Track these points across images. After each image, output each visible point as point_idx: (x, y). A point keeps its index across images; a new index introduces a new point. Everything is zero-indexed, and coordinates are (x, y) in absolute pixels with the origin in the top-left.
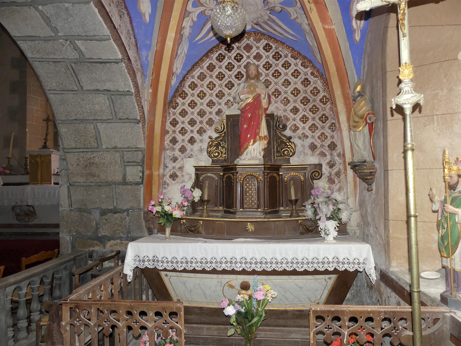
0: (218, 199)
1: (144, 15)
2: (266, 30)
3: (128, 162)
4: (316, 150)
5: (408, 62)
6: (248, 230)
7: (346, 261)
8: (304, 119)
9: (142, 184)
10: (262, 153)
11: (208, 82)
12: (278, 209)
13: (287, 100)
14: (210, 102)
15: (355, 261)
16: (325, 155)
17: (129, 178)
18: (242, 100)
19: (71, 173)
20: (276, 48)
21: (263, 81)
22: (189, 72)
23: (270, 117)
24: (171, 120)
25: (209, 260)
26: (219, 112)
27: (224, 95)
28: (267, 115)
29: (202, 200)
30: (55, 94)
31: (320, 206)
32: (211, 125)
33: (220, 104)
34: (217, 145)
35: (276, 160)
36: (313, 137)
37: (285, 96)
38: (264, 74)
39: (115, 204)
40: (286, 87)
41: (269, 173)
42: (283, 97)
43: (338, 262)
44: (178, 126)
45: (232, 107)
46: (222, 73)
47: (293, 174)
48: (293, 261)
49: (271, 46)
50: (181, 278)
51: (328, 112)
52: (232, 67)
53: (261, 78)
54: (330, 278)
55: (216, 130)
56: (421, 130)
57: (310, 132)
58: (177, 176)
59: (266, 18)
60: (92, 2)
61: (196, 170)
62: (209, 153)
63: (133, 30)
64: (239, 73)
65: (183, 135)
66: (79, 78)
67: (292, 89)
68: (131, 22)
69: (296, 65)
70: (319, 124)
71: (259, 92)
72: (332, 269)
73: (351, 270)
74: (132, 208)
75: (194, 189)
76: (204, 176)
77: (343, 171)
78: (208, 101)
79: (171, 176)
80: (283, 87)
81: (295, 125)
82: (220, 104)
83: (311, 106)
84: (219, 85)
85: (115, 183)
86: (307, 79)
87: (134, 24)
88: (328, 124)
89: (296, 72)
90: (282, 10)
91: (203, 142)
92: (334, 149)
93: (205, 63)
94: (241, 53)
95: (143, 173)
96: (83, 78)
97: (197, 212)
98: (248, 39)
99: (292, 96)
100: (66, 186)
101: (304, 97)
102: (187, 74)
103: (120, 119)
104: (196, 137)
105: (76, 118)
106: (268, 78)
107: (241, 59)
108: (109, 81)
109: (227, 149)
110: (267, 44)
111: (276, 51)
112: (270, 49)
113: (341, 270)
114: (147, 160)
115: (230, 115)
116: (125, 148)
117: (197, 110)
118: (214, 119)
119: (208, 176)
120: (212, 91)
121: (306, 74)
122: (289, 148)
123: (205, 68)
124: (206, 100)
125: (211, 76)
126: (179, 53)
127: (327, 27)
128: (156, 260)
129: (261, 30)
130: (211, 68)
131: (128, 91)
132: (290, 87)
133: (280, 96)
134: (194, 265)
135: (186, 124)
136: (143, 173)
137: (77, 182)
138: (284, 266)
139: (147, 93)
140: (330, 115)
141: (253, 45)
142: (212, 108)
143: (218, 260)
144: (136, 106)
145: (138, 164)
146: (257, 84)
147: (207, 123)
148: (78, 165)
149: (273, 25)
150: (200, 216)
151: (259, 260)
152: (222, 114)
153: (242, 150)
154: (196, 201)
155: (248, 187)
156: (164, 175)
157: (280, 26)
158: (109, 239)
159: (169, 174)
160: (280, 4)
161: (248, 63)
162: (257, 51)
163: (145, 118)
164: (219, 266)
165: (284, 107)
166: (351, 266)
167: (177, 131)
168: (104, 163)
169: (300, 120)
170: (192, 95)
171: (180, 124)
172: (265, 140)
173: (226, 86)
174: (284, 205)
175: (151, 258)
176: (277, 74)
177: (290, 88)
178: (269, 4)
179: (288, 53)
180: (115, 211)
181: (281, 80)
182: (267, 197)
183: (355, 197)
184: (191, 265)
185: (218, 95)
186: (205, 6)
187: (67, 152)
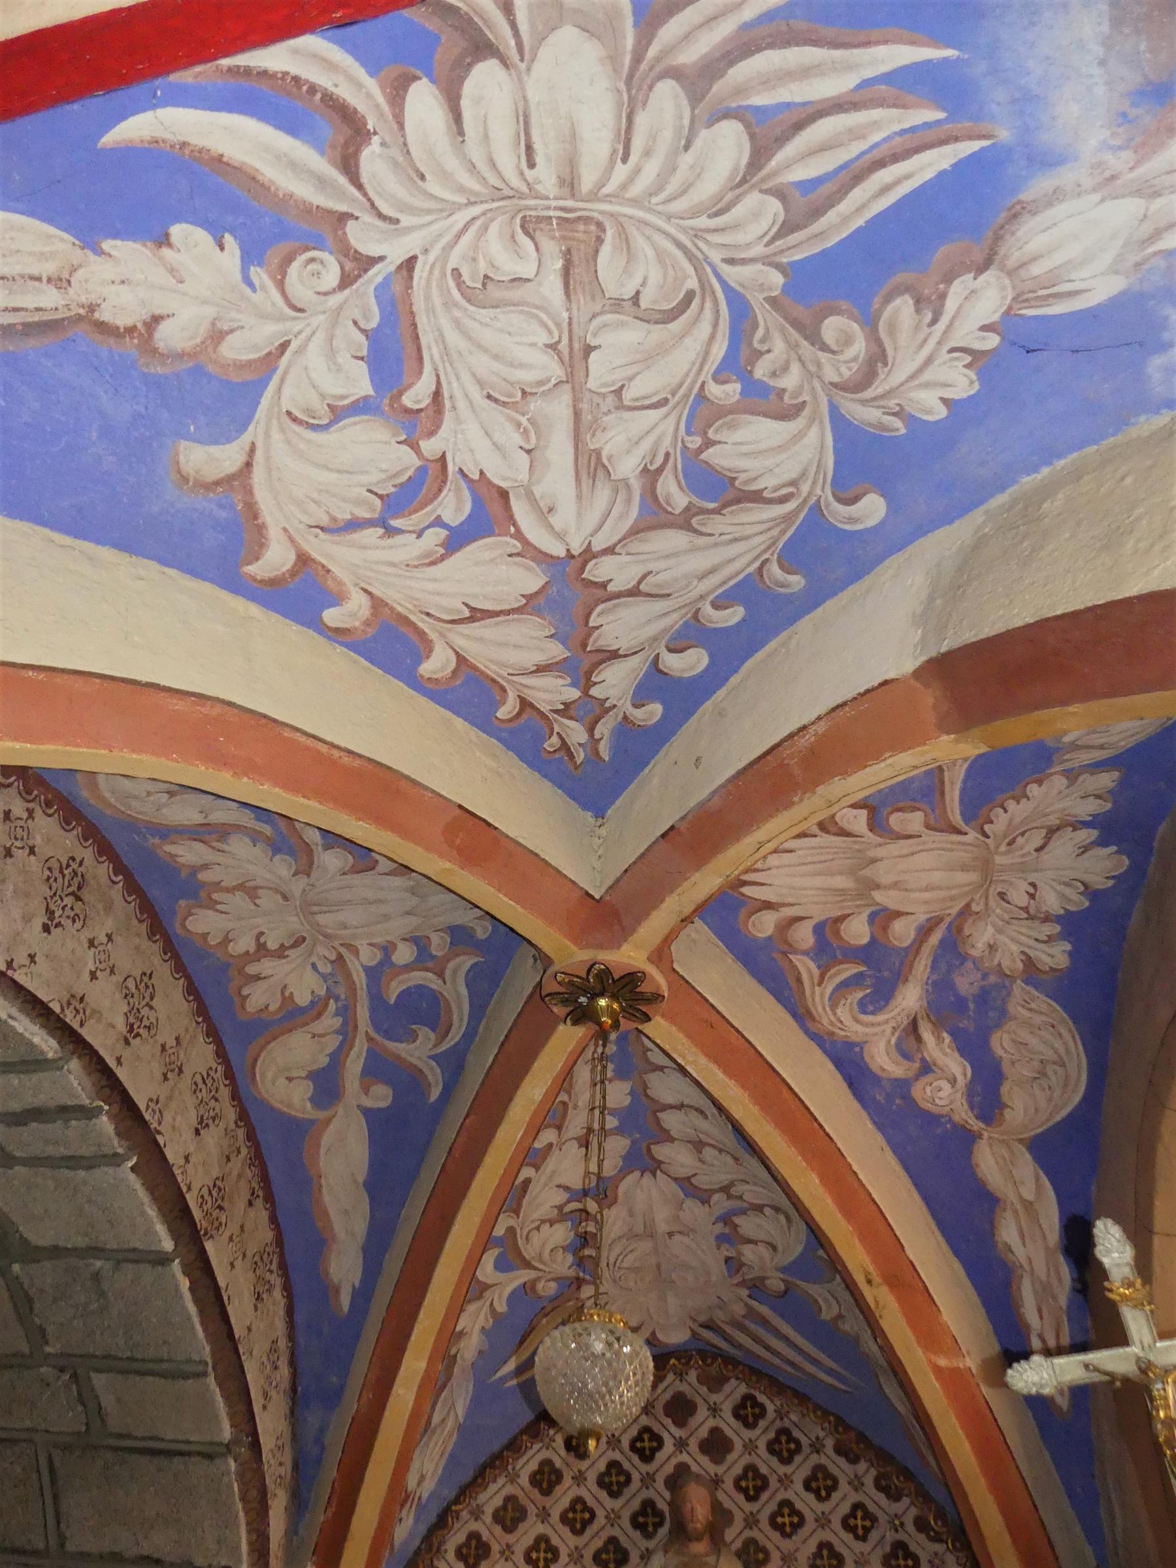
1: (337, 1291)
2: (740, 1346)
20: (780, 1415)
21: (738, 1544)
22: (466, 1491)
52: (615, 1488)
59: (739, 1310)
60: (177, 1261)
63: (291, 1337)
69: (857, 1484)
87: (299, 1318)
90: (786, 1292)
93: (525, 1458)
94: (657, 1428)
98: (681, 1375)
102: (457, 1501)
106: (754, 1533)
107: (654, 1451)
111: (778, 1424)
123: (524, 1480)
125: (544, 1515)
126: (436, 1419)
127: (943, 1362)
141: (699, 1401)
149: (761, 1332)
160: (784, 1270)
162: (711, 1423)
178: (745, 1269)
179: (822, 1434)
186: (536, 1269)
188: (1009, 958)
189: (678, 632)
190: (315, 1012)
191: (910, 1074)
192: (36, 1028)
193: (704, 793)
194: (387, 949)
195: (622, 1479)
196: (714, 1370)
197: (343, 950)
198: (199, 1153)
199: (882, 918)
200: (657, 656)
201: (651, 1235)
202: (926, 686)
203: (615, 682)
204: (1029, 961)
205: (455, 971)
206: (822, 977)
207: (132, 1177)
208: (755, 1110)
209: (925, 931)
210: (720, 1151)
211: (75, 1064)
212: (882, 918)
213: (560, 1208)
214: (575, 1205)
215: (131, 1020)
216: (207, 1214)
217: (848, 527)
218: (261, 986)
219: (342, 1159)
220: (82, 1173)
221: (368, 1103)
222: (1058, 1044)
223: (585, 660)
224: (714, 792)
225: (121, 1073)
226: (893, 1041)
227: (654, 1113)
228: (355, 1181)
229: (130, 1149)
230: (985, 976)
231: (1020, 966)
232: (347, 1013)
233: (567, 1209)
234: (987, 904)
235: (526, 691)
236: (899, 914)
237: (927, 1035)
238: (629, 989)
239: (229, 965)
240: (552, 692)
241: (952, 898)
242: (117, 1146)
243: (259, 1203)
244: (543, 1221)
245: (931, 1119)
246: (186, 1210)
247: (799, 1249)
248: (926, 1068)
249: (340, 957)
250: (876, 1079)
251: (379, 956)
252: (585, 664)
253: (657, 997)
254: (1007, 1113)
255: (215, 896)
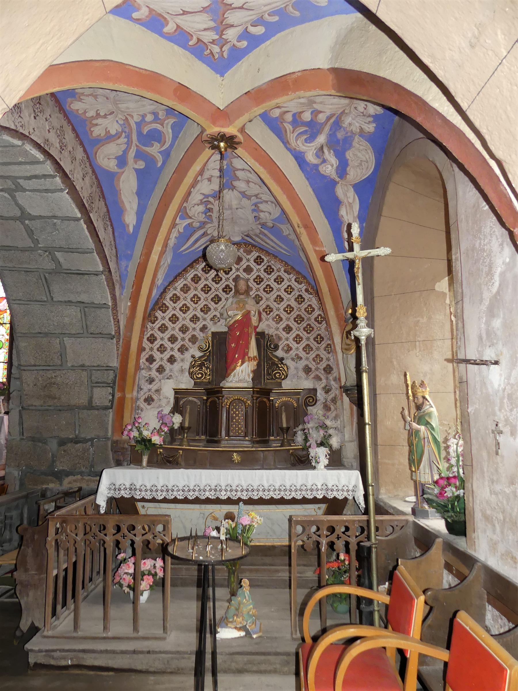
0: (201, 426)
1: (128, 226)
2: (258, 242)
3: (97, 383)
4: (310, 373)
5: (362, 303)
6: (234, 461)
7: (335, 488)
8: (298, 339)
9: (111, 408)
10: (251, 375)
11: (192, 295)
12: (267, 438)
13: (280, 317)
14: (193, 316)
15: (344, 488)
16: (321, 379)
17: (97, 402)
18: (230, 317)
19: (26, 395)
21: (254, 296)
22: (171, 283)
23: (261, 336)
24: (148, 335)
25: (191, 488)
26: (204, 329)
27: (210, 309)
28: (257, 334)
29: (182, 427)
30: (19, 304)
31: (311, 431)
32: (194, 343)
33: (205, 319)
34: (201, 366)
35: (266, 383)
36: (307, 359)
37: (277, 313)
38: (254, 289)
39: (77, 432)
40: (279, 304)
41: (258, 397)
42: (275, 314)
43: (327, 490)
44: (156, 343)
45: (219, 324)
46: (208, 285)
47: (284, 399)
48: (281, 488)
49: (263, 259)
50: (159, 509)
51: (323, 332)
53: (251, 293)
54: (319, 508)
55: (200, 349)
56: (405, 355)
57: (304, 353)
58: (153, 400)
59: (258, 231)
61: (176, 393)
62: (191, 374)
63: (114, 240)
64: (227, 286)
65: (161, 353)
66: (51, 288)
67: (285, 306)
68: (113, 233)
69: (290, 280)
70: (314, 344)
71: (248, 309)
72: (321, 497)
73: (341, 498)
74: (98, 438)
75: (174, 414)
76: (184, 400)
77: (340, 396)
78: (191, 316)
79: (146, 400)
80: (275, 303)
81: (288, 345)
82: (205, 319)
83: (305, 325)
84: (205, 299)
85: (79, 407)
86: (301, 296)
87: (116, 234)
88: (323, 345)
89: (289, 288)
91: (185, 361)
92: (330, 373)
95: (113, 396)
96: (56, 288)
97: (175, 441)
99: (285, 313)
100: (18, 410)
101: (298, 315)
102: (169, 285)
103: (91, 333)
104: (176, 356)
105: (40, 331)
106: (259, 293)
108: (84, 292)
109: (212, 370)
110: (258, 257)
111: (267, 264)
112: (261, 262)
113: (329, 498)
114: (120, 379)
115: (217, 332)
116: (94, 366)
117: (178, 325)
118: (198, 336)
119: (190, 401)
120: (197, 305)
121: (300, 290)
122: (281, 370)
123: (189, 279)
124: (190, 314)
127: (317, 249)
128: (133, 488)
129: (252, 241)
130: (196, 279)
131: (105, 304)
132: (282, 303)
133: (271, 313)
134: (175, 493)
135: (166, 340)
136: (113, 396)
137: (32, 405)
138: (272, 494)
139: (124, 306)
140: (326, 336)
141: (243, 257)
142: (195, 323)
143: (202, 488)
144: (112, 320)
145: (108, 385)
146: (246, 300)
147: (189, 340)
148: (35, 385)
149: (264, 238)
150: (179, 445)
151: (245, 488)
152: (207, 330)
153: (229, 371)
154: (176, 428)
155: (234, 413)
156: (138, 399)
157: (272, 241)
158: (68, 474)
159: (143, 398)
160: (272, 220)
161: (238, 276)
162: (247, 264)
163: (120, 334)
164: (202, 494)
165: (276, 325)
166: (340, 493)
167: (155, 348)
168: (67, 383)
169: (294, 340)
170: (173, 308)
171: (159, 340)
172: (255, 361)
173: (212, 299)
174: (275, 434)
175: (128, 486)
176: (269, 289)
177: (283, 305)
179: (281, 267)
180: (76, 441)
181: (273, 295)
182: (255, 425)
183: (352, 424)
184: (172, 493)
185: (203, 309)
187: (24, 370)
188: (355, 128)
189: (255, 21)
190: (117, 137)
191: (319, 163)
192: (37, 152)
193: (261, 83)
194: (144, 116)
195: (219, 279)
196: (248, 249)
197: (128, 116)
198: (85, 186)
199: (316, 113)
200: (247, 27)
201: (231, 209)
202: (331, 74)
203: (231, 34)
204: (361, 129)
205: (167, 124)
206: (294, 131)
207: (67, 195)
208: (268, 176)
209: (328, 119)
210: (255, 184)
211: (49, 162)
212: (316, 113)
213: (201, 200)
214: (206, 199)
215: (61, 144)
216: (89, 205)
217: (316, 4)
218: (98, 127)
219: (128, 185)
220: (50, 194)
221: (136, 167)
222: (367, 157)
223: (221, 27)
224: (264, 84)
225: (62, 163)
226: (315, 152)
227: (234, 171)
228: (133, 193)
229: (66, 187)
230: (347, 133)
231: (358, 130)
232: (129, 137)
233: (203, 201)
234: (350, 110)
235: (201, 36)
236: (321, 112)
237: (326, 150)
238: (231, 142)
239: (86, 120)
240: (209, 36)
241: (339, 108)
242: (62, 186)
243: (101, 199)
244: (195, 204)
245: (324, 177)
246: (84, 205)
247: (279, 214)
248: (324, 161)
249: (127, 118)
250: (307, 164)
251: (141, 119)
252: (221, 28)
253: (239, 143)
254: (348, 176)
255: (81, 97)
